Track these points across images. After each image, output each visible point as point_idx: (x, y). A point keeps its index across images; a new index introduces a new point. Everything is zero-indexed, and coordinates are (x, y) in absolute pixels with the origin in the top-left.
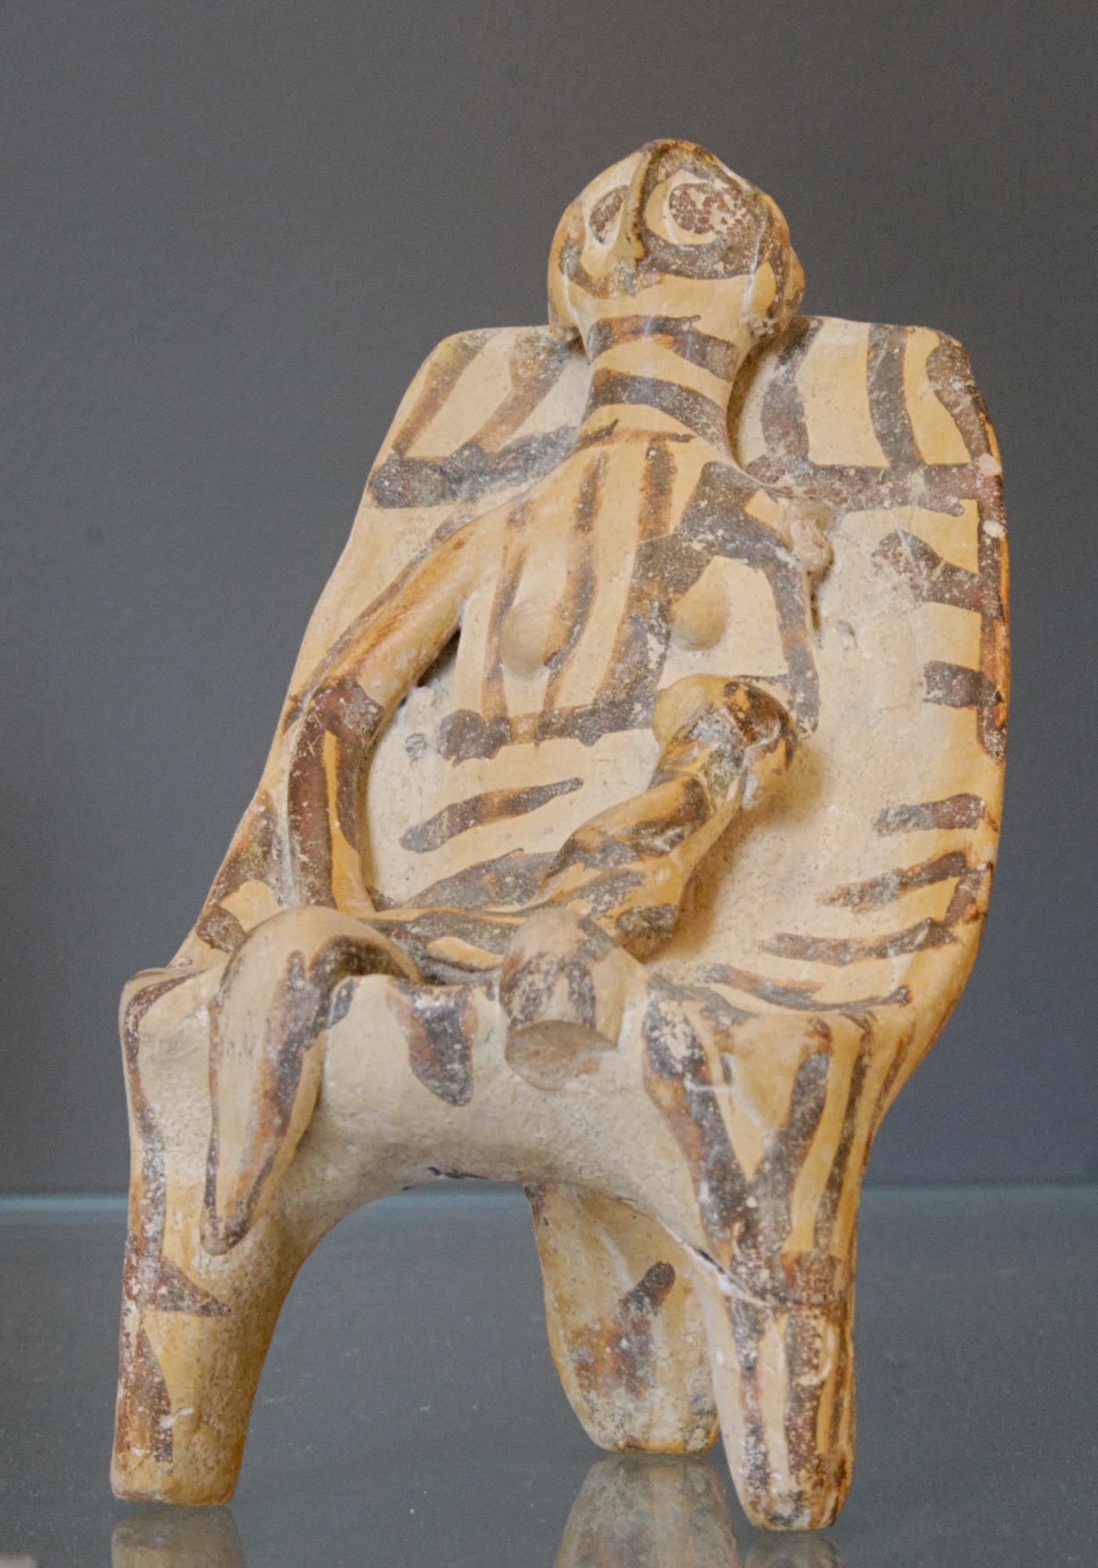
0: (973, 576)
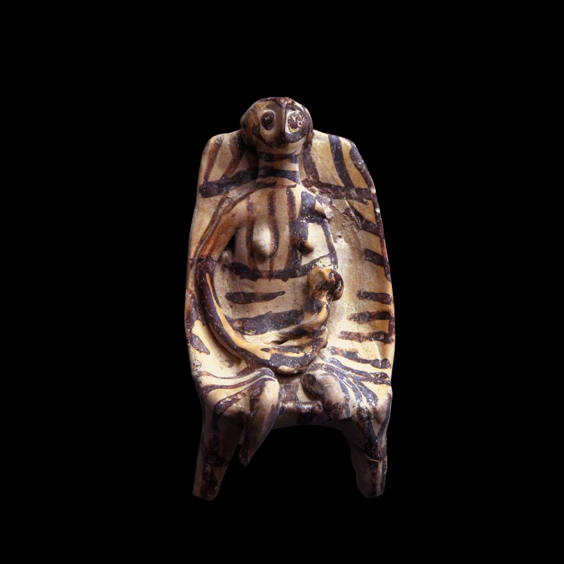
0: (375, 225)
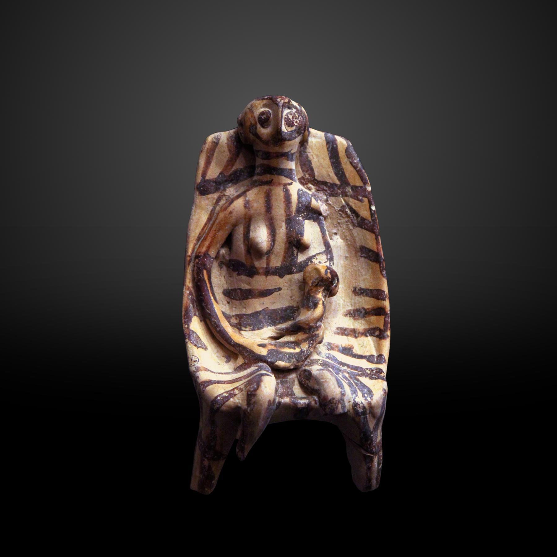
0: (370, 222)
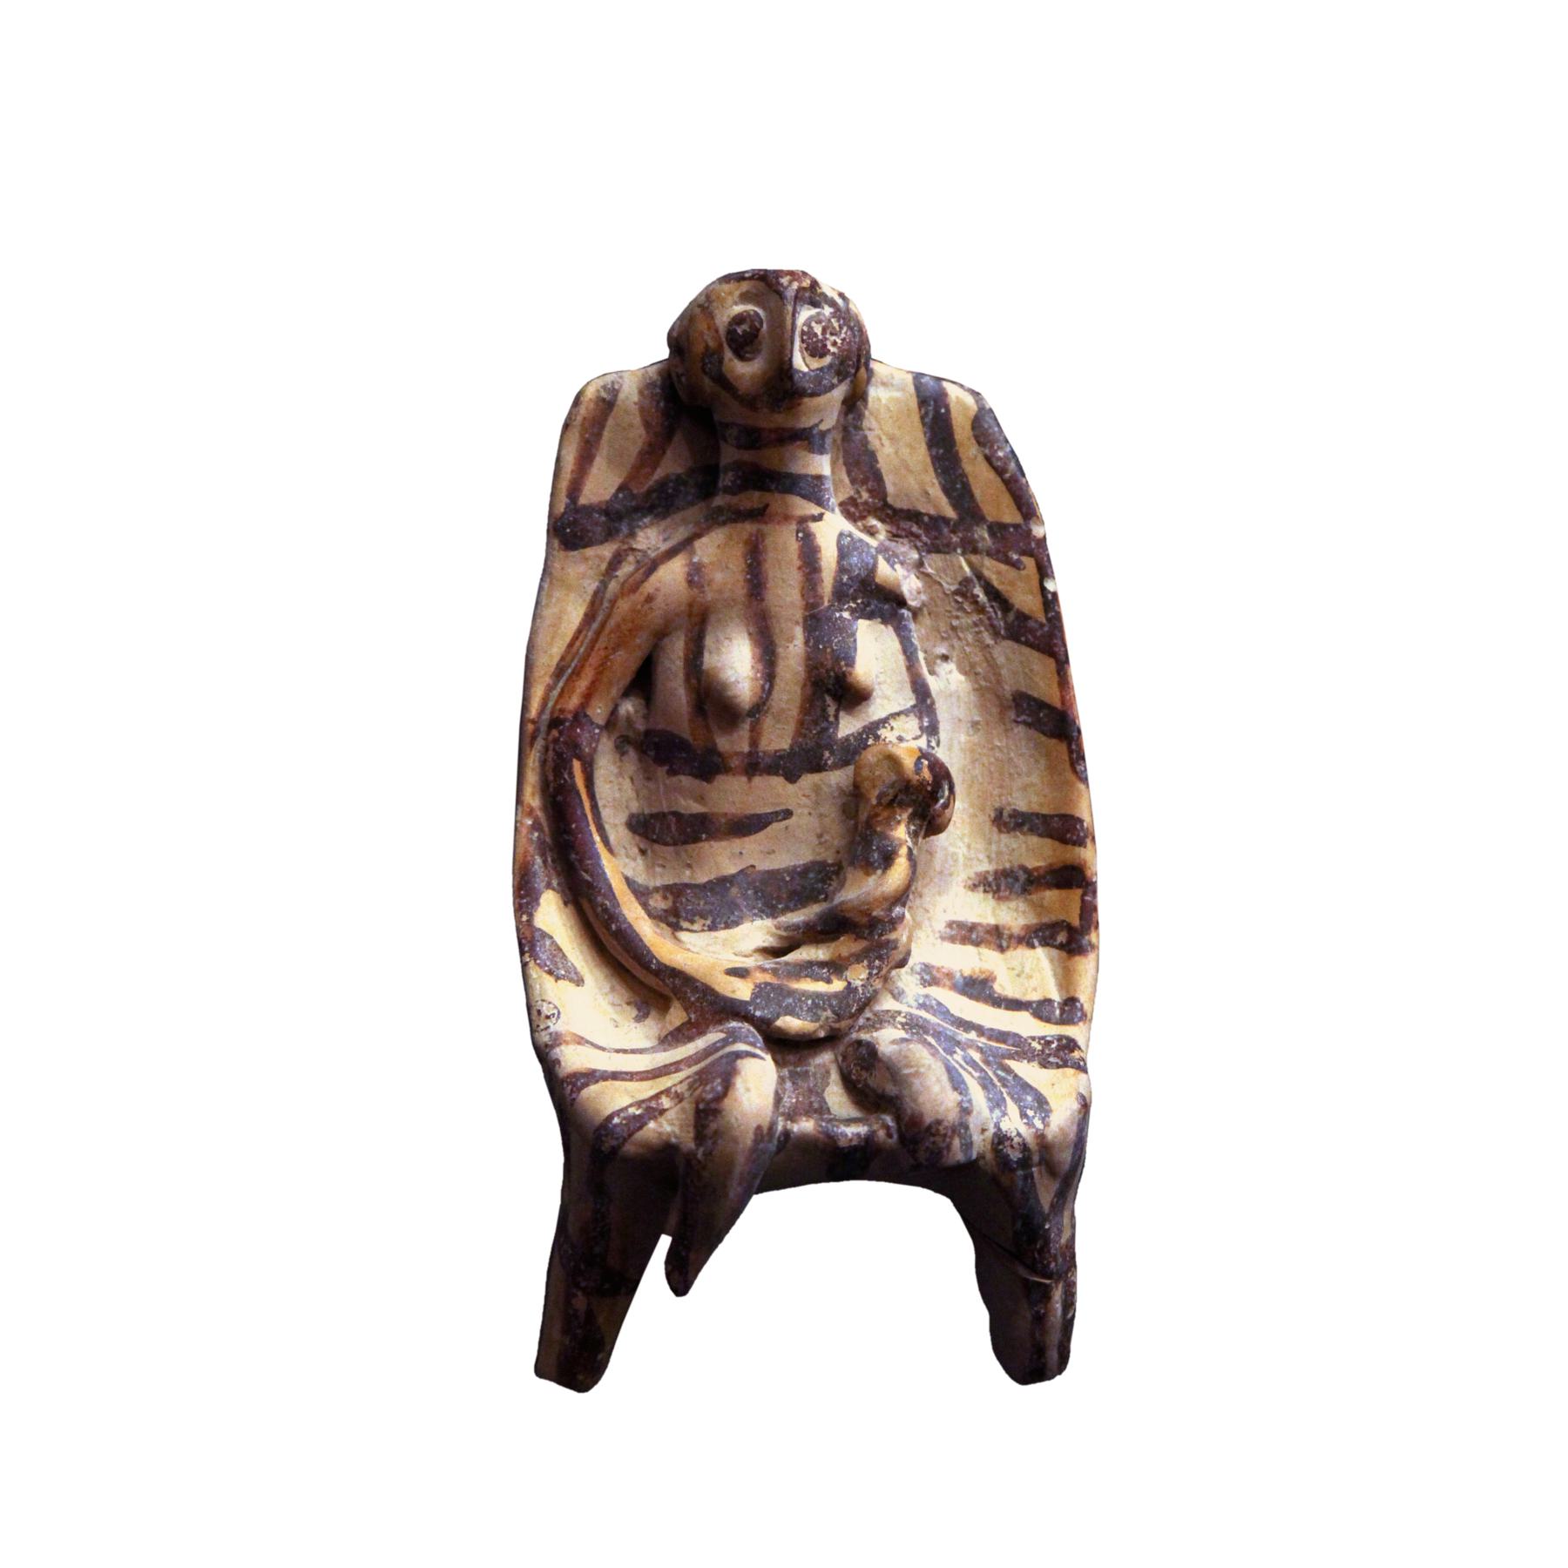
0: (1042, 625)
